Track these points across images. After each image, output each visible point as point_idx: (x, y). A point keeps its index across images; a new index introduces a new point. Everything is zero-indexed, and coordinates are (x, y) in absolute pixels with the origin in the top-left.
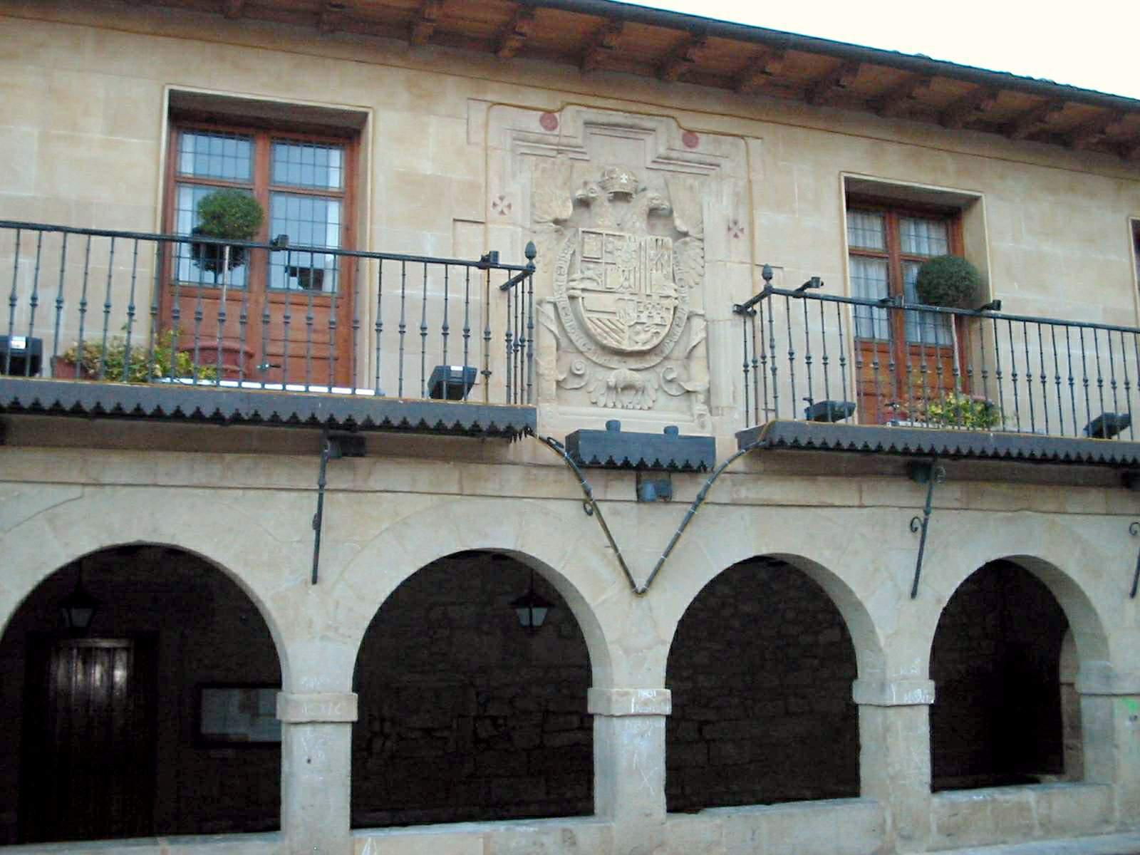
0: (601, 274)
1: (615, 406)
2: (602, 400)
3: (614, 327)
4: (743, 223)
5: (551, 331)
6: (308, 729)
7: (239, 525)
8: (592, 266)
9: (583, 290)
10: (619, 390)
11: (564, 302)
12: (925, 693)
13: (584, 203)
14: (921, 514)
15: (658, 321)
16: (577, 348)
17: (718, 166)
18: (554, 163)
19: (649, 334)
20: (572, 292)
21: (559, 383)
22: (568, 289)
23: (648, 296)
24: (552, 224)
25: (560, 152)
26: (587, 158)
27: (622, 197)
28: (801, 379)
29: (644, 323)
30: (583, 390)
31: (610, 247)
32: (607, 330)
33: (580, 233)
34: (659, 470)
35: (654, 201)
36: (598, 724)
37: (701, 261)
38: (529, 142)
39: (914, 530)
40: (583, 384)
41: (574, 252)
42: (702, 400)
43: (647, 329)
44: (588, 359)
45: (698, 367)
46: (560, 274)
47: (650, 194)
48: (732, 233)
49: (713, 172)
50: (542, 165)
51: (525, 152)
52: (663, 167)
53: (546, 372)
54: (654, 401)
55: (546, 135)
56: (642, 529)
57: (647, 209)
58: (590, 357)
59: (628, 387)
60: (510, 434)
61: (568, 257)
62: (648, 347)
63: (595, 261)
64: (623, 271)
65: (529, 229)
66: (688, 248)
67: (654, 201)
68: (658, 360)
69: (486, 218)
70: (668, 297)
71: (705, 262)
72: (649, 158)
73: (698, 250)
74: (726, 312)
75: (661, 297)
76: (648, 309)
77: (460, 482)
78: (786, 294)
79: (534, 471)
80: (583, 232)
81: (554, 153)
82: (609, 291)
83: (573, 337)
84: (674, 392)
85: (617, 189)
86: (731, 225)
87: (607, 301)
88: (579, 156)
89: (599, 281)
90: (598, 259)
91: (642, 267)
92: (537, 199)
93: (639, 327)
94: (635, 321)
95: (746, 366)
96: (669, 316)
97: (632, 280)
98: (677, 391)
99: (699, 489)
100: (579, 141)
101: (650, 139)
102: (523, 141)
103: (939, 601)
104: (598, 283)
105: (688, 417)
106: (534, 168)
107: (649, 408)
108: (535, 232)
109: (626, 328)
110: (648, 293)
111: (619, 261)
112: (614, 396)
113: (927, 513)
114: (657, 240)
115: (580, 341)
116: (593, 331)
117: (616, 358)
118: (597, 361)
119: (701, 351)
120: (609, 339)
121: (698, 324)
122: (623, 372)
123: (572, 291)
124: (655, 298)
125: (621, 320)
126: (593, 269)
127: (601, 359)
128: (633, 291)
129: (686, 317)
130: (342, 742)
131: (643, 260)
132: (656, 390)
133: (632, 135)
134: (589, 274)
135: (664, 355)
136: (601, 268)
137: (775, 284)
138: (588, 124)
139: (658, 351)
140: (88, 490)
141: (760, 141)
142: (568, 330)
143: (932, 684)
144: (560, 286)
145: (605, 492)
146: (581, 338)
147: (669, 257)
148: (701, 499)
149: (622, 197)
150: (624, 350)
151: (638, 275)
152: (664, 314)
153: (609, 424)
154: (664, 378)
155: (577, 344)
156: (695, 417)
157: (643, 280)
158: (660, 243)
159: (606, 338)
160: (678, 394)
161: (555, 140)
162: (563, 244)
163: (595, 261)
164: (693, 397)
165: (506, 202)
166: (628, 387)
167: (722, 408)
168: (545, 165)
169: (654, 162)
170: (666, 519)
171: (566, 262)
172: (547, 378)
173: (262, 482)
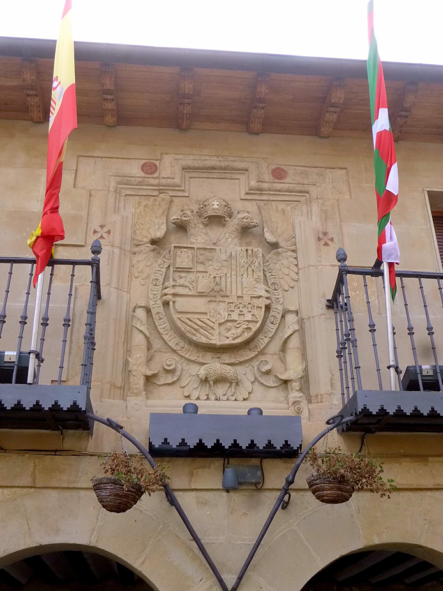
0: (193, 282)
1: (208, 399)
3: (204, 325)
4: (332, 232)
5: (141, 331)
8: (183, 275)
9: (175, 295)
10: (212, 383)
11: (157, 308)
13: (181, 227)
15: (249, 317)
16: (171, 348)
17: (307, 192)
18: (155, 200)
19: (239, 331)
21: (148, 379)
22: (162, 296)
24: (149, 245)
25: (161, 191)
26: (187, 195)
27: (216, 220)
29: (236, 321)
30: (177, 385)
31: (202, 258)
32: (197, 327)
33: (172, 249)
34: (244, 458)
35: (245, 220)
37: (295, 269)
38: (132, 185)
40: (175, 379)
41: (169, 266)
42: (298, 388)
43: (238, 326)
45: (293, 358)
46: (155, 285)
48: (323, 242)
49: (304, 198)
50: (144, 203)
51: (129, 193)
52: (256, 197)
53: (135, 367)
54: (249, 393)
55: (146, 178)
57: (238, 227)
58: (182, 354)
59: (220, 380)
61: (164, 270)
63: (187, 270)
64: (215, 277)
65: (130, 251)
66: (280, 258)
67: (245, 220)
68: (252, 354)
69: (85, 243)
71: (299, 269)
72: (243, 192)
73: (293, 260)
74: (318, 307)
75: (251, 297)
76: (239, 308)
77: (33, 476)
78: (364, 273)
80: (175, 247)
81: (156, 193)
83: (166, 337)
84: (271, 384)
85: (210, 213)
86: (321, 236)
88: (180, 194)
89: (191, 286)
90: (191, 268)
91: (233, 273)
92: (138, 227)
93: (229, 324)
94: (226, 319)
96: (260, 314)
98: (274, 382)
100: (177, 181)
101: (243, 178)
102: (127, 184)
104: (190, 289)
105: (284, 405)
106: (137, 205)
109: (216, 326)
110: (238, 295)
111: (210, 269)
112: (207, 389)
114: (247, 250)
115: (173, 341)
116: (183, 329)
118: (190, 358)
119: (294, 342)
120: (198, 335)
121: (291, 318)
122: (216, 366)
123: (164, 297)
125: (211, 319)
126: (186, 277)
129: (280, 315)
131: (234, 267)
132: (252, 383)
133: (228, 176)
134: (181, 281)
136: (191, 276)
138: (185, 169)
139: (252, 345)
141: (344, 171)
142: (161, 331)
145: (190, 481)
146: (175, 337)
147: (259, 264)
150: (214, 345)
152: (255, 312)
154: (259, 369)
155: (170, 344)
156: (290, 404)
157: (234, 285)
158: (250, 252)
159: (195, 335)
160: (275, 385)
161: (156, 182)
162: (160, 261)
163: (187, 270)
165: (105, 229)
166: (220, 380)
167: (321, 395)
168: (147, 202)
169: (247, 194)
171: (162, 275)
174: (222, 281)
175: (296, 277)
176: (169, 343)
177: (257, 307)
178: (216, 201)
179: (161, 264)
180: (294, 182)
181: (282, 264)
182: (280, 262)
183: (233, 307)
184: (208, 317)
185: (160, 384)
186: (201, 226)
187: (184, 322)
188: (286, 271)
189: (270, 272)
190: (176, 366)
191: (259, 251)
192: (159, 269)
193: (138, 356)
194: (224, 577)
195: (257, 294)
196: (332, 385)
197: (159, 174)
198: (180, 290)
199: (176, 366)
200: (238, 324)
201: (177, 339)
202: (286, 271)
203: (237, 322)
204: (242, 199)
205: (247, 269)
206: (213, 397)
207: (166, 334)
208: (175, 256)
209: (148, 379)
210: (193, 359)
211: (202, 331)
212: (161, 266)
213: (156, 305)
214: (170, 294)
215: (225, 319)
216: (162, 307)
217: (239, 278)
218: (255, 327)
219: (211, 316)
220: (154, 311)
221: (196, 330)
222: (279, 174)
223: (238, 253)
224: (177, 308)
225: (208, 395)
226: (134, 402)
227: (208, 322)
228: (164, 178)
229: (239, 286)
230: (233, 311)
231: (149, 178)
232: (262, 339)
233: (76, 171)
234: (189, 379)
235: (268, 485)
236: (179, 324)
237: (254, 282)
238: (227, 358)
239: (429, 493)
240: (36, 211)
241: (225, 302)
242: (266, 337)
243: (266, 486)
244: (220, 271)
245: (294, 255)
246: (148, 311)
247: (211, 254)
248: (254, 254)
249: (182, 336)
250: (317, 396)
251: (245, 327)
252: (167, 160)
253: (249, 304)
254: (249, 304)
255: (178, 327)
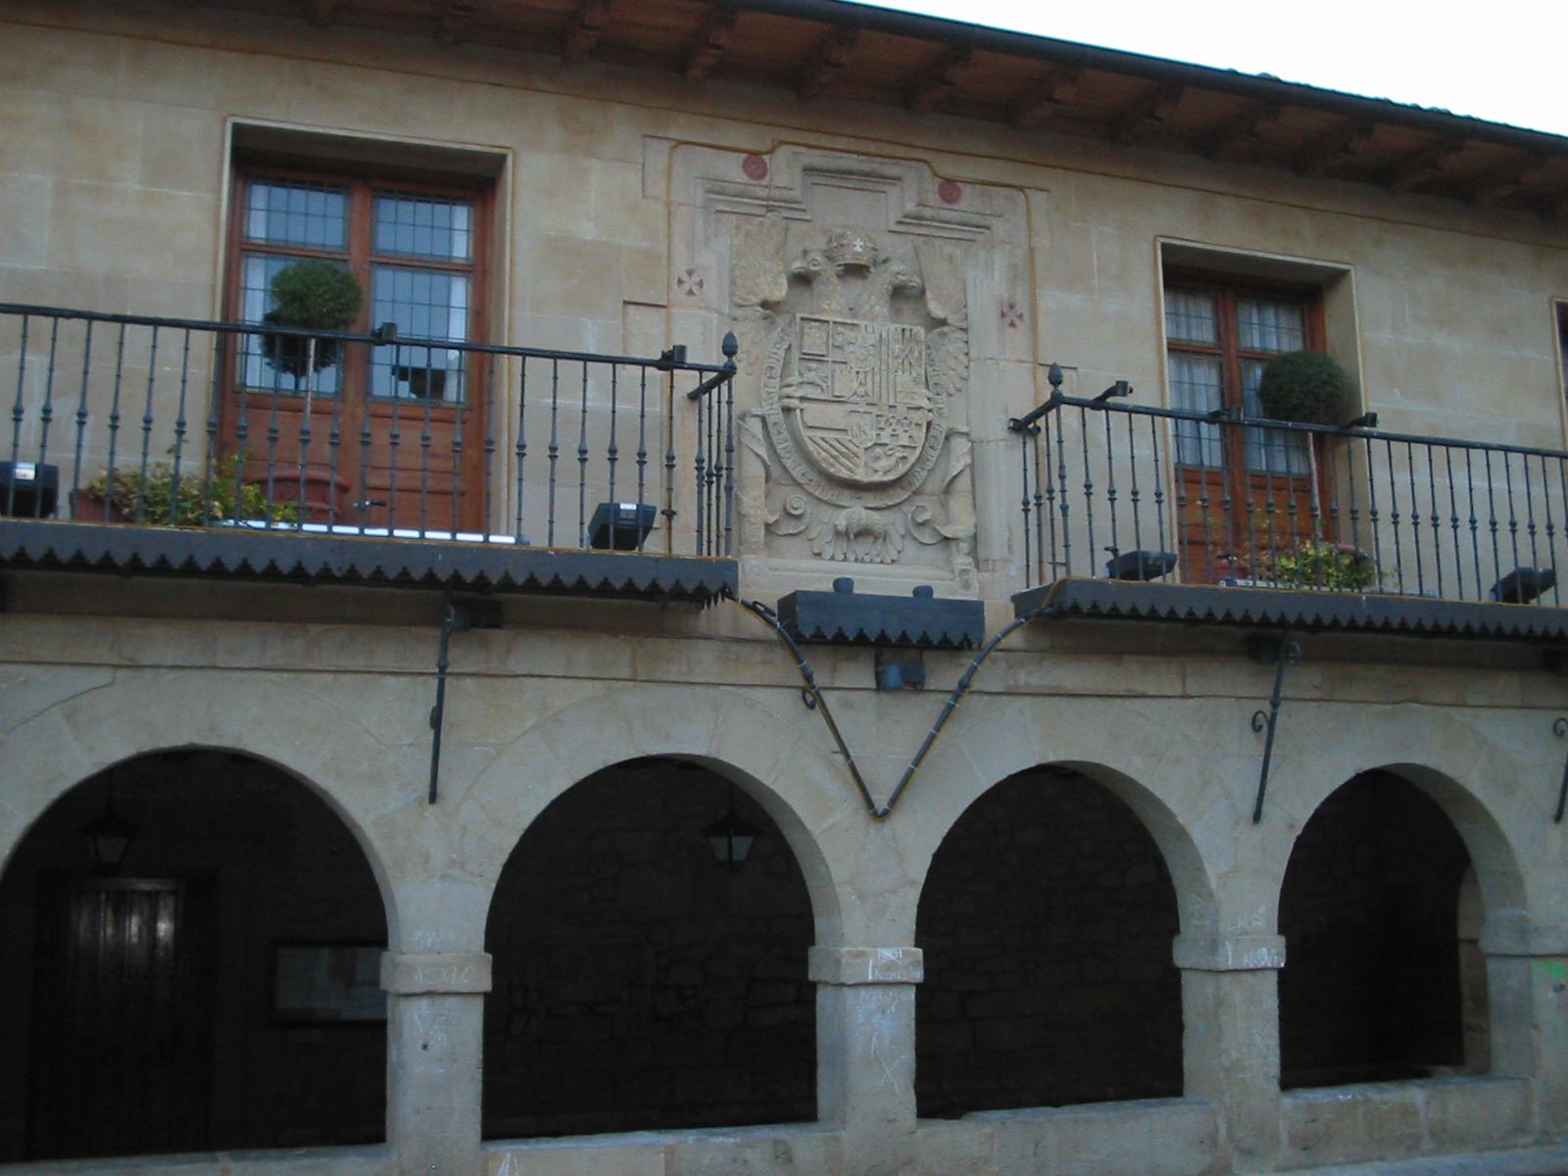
0: (827, 377)
1: (845, 559)
2: (829, 551)
3: (844, 450)
4: (1022, 307)
6: (424, 1002)
7: (333, 725)
8: (813, 365)
9: (802, 399)
10: (852, 536)
11: (776, 417)
12: (1271, 953)
13: (802, 280)
14: (1266, 707)
17: (988, 228)
18: (762, 224)
19: (893, 460)
20: (786, 402)
21: (769, 528)
23: (891, 407)
24: (759, 308)
25: (770, 209)
26: (808, 217)
27: (855, 271)
28: (1103, 524)
29: (886, 445)
31: (839, 339)
32: (835, 453)
34: (908, 646)
35: (901, 278)
36: (823, 996)
37: (965, 360)
38: (727, 195)
39: (1257, 729)
40: (802, 528)
42: (966, 551)
43: (890, 453)
44: (809, 494)
45: (959, 505)
47: (894, 267)
51: (722, 208)
52: (911, 229)
53: (752, 511)
54: (899, 552)
55: (750, 185)
56: (883, 729)
58: (811, 491)
60: (701, 597)
61: (782, 353)
62: (891, 477)
63: (819, 359)
64: (858, 373)
65: (729, 316)
70: (919, 408)
71: (969, 361)
72: (893, 217)
73: (961, 344)
74: (996, 429)
75: (909, 408)
78: (1082, 404)
79: (735, 648)
80: (802, 319)
81: (762, 211)
82: (838, 401)
83: (788, 464)
84: (927, 539)
85: (849, 260)
86: (1006, 309)
87: (835, 415)
89: (824, 386)
90: (823, 356)
91: (883, 367)
92: (738, 273)
93: (879, 450)
95: (1026, 503)
97: (870, 385)
99: (960, 673)
100: (796, 194)
101: (893, 192)
102: (720, 194)
103: (1291, 826)
104: (822, 390)
105: (948, 575)
106: (734, 231)
107: (893, 561)
108: (736, 320)
110: (891, 404)
112: (845, 545)
113: (1275, 705)
114: (903, 330)
115: (798, 470)
117: (847, 493)
118: (821, 497)
119: (964, 483)
121: (960, 445)
122: (856, 512)
124: (902, 410)
125: (854, 441)
127: (828, 494)
128: (870, 400)
130: (470, 1021)
131: (885, 357)
132: (903, 536)
133: (870, 186)
134: (811, 376)
135: (914, 489)
136: (827, 369)
137: (1065, 390)
138: (809, 170)
140: (122, 674)
142: (782, 453)
143: (1281, 941)
144: (770, 393)
146: (800, 465)
147: (920, 353)
148: (964, 686)
149: (855, 271)
151: (877, 378)
152: (914, 432)
153: (837, 583)
154: (913, 519)
155: (795, 474)
156: (957, 573)
157: (884, 385)
158: (908, 333)
159: (833, 466)
161: (762, 193)
163: (819, 359)
164: (953, 545)
165: (696, 278)
166: (865, 533)
167: (994, 561)
168: (749, 227)
169: (899, 223)
170: (915, 715)
172: (752, 520)
173: (360, 662)
174: (868, 380)
175: (965, 374)
176: (792, 472)
177: (917, 424)
178: (858, 240)
179: (777, 343)
180: (971, 209)
181: (948, 352)
182: (944, 348)
183: (883, 423)
184: (850, 438)
185: (781, 533)
186: (835, 280)
187: (817, 444)
188: (952, 363)
189: (931, 365)
190: (805, 511)
191: (920, 331)
192: (775, 351)
193: (756, 493)
194: (874, 797)
195: (916, 404)
196: (1010, 547)
197: (771, 179)
198: (809, 392)
199: (805, 511)
200: (890, 449)
201: (804, 468)
202: (952, 363)
203: (890, 447)
204: (890, 231)
205: (903, 362)
206: (852, 557)
207: (789, 458)
208: (802, 334)
209: (769, 528)
210: (826, 499)
211: (842, 459)
212: (778, 346)
213: (772, 412)
214: (796, 398)
215: (873, 442)
216: (781, 414)
217: (891, 377)
218: (913, 457)
219: (853, 437)
220: (770, 422)
221: (834, 458)
222: (949, 190)
223: (891, 333)
224: (805, 419)
225: (845, 554)
226: (754, 562)
227: (851, 446)
228: (778, 188)
229: (891, 391)
230: (883, 429)
231: (755, 185)
232: (919, 472)
233: (643, 165)
234: (819, 529)
235: (932, 683)
236: (811, 447)
237: (912, 384)
238: (871, 500)
239: (1118, 701)
240: (589, 238)
241: (870, 413)
242: (923, 469)
243: (926, 687)
244: (865, 363)
245: (963, 336)
246: (764, 419)
247: (853, 334)
248: (913, 338)
249: (811, 462)
250: (987, 561)
251: (901, 455)
252: (783, 152)
253: (905, 418)
254: (905, 418)
255: (809, 452)
